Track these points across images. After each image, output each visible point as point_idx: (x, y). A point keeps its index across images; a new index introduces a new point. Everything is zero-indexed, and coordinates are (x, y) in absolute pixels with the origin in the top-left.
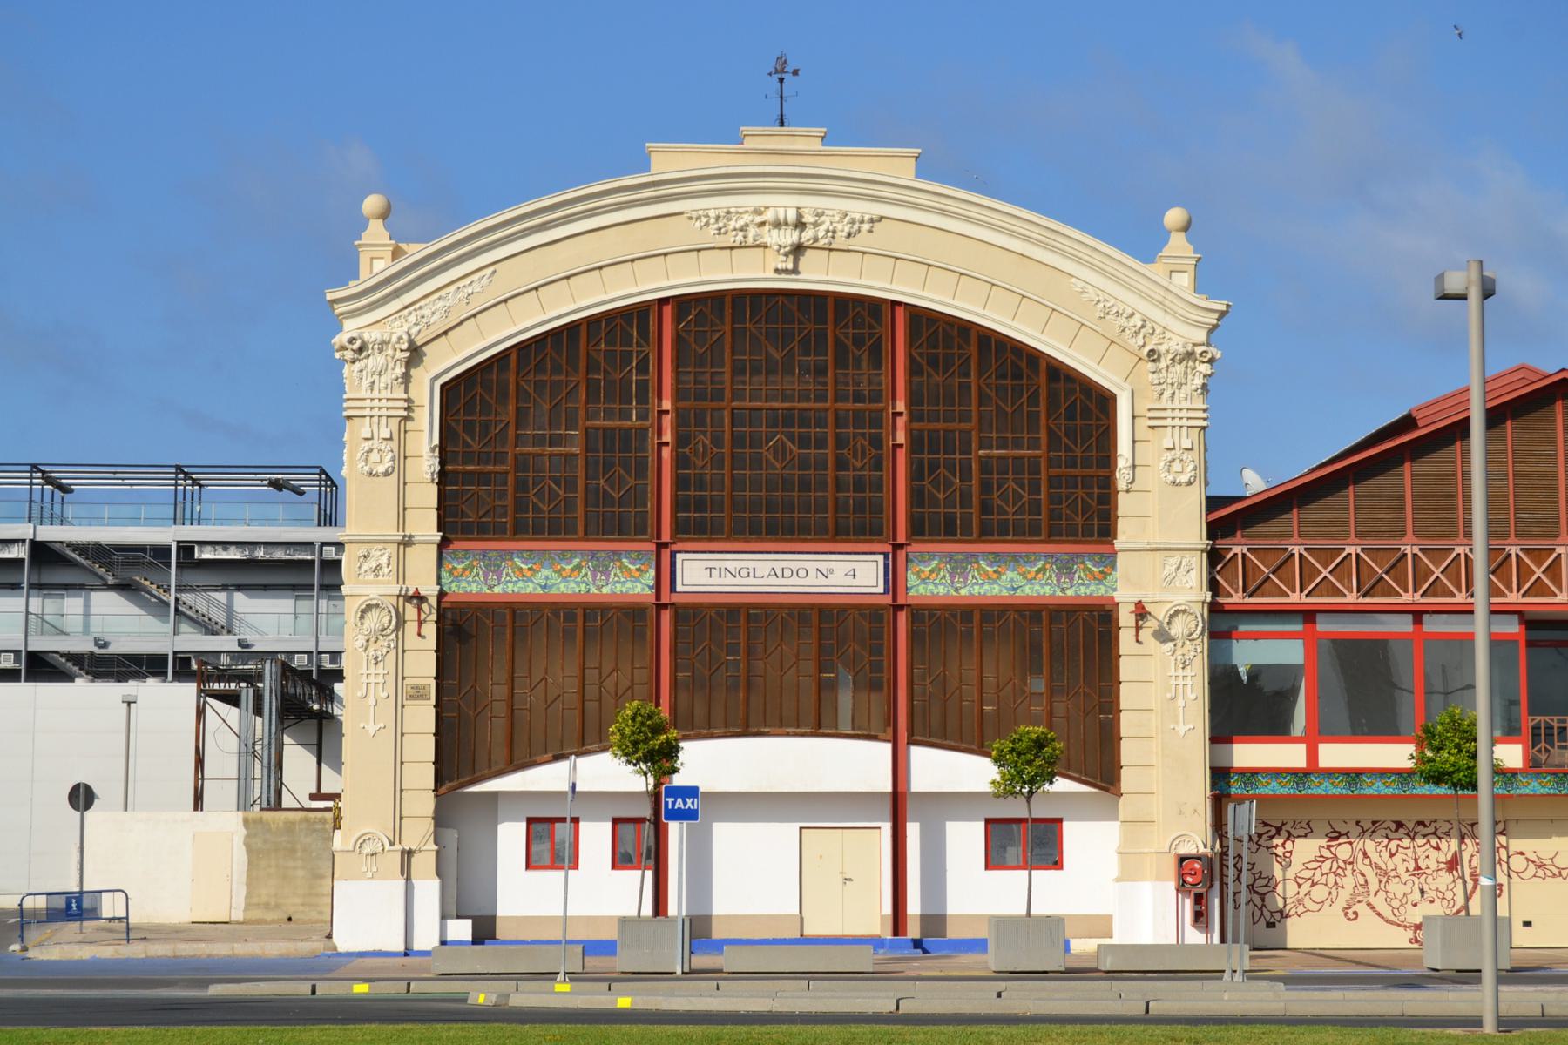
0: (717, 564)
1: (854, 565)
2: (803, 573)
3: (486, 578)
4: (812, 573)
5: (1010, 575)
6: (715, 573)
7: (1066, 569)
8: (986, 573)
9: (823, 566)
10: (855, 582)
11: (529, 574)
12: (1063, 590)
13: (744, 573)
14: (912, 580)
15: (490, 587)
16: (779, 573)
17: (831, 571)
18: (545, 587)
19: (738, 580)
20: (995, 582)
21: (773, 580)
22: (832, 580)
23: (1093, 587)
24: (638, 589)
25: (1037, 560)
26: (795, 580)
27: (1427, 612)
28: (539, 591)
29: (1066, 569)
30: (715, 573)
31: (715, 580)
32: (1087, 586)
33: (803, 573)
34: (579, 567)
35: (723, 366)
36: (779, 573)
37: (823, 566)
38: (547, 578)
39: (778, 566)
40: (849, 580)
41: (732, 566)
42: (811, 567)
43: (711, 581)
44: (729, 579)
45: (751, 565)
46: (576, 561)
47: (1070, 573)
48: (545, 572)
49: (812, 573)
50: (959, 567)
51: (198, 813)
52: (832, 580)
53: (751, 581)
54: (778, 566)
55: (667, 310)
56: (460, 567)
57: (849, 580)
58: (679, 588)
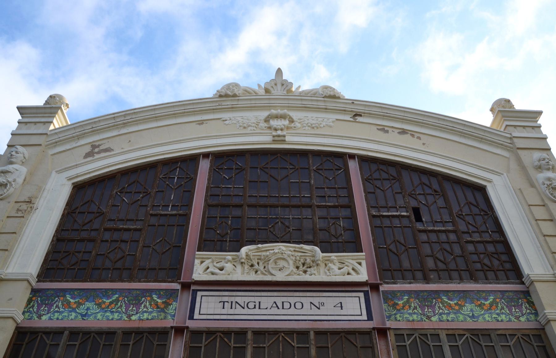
1: (341, 300)
2: (299, 305)
3: (127, 309)
4: (307, 305)
9: (316, 301)
11: (457, 308)
13: (251, 305)
16: (280, 306)
17: (323, 304)
19: (246, 311)
20: (74, 310)
21: (275, 311)
22: (323, 310)
26: (292, 311)
29: (136, 298)
32: (150, 313)
33: (299, 305)
34: (117, 300)
36: (280, 306)
37: (316, 301)
38: (88, 309)
39: (279, 301)
40: (338, 311)
42: (306, 301)
43: (224, 311)
44: (239, 310)
45: (257, 300)
46: (491, 298)
47: (138, 305)
48: (88, 304)
49: (307, 305)
50: (427, 299)
53: (257, 311)
54: (279, 301)
55: (204, 166)
56: (400, 302)
58: (196, 316)
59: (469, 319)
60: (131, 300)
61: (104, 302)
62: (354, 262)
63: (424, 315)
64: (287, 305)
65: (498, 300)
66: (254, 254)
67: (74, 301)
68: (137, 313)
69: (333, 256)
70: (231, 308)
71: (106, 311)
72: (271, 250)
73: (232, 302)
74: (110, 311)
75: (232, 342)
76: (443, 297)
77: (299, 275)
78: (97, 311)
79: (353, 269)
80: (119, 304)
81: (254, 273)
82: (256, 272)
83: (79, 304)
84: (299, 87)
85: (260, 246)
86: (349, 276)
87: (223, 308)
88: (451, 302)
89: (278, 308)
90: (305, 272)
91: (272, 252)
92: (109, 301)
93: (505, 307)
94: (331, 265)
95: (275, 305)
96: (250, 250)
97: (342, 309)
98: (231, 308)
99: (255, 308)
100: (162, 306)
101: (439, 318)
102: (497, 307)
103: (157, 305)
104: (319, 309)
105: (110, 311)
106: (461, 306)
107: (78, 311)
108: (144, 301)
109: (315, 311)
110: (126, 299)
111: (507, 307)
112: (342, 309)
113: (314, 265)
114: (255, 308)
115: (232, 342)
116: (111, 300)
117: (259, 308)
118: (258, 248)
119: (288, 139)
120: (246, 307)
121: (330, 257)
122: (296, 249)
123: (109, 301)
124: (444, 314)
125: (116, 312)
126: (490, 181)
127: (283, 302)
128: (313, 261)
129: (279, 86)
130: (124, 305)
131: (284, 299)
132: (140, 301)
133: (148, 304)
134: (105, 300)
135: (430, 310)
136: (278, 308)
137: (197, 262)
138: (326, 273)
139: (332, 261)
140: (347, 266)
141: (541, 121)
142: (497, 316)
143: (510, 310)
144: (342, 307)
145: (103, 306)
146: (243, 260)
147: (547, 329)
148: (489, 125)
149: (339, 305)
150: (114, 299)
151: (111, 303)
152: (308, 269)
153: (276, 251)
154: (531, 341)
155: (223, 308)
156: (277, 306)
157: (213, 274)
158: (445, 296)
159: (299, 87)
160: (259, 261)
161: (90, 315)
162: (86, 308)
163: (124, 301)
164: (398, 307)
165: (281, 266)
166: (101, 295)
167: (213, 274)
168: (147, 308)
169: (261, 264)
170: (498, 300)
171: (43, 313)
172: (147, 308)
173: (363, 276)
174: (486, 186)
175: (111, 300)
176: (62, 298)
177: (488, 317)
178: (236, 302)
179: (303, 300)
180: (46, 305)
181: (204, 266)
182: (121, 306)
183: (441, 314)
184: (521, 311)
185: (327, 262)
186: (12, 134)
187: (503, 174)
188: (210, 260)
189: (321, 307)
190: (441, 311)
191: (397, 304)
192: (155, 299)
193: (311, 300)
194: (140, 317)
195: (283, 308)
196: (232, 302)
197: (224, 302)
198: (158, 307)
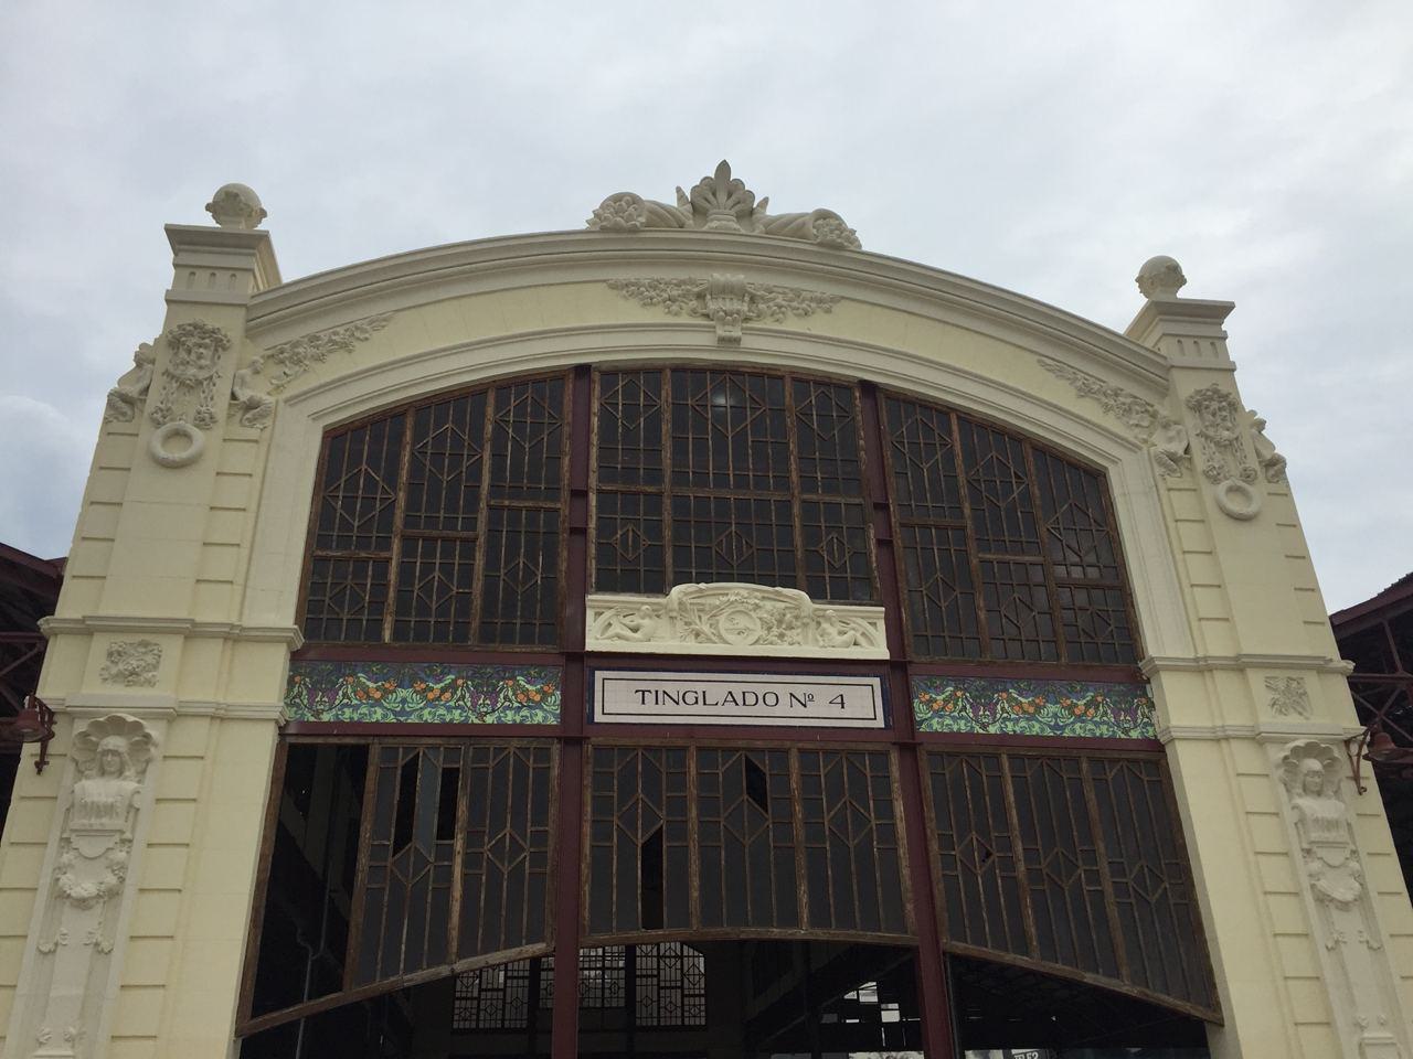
0: (653, 686)
2: (771, 700)
4: (785, 699)
5: (1052, 708)
6: (650, 698)
7: (983, 701)
8: (526, 692)
9: (799, 691)
10: (846, 713)
12: (317, 713)
13: (690, 698)
14: (921, 711)
15: (481, 716)
16: (740, 700)
18: (403, 712)
19: (683, 708)
20: (377, 703)
21: (730, 708)
22: (811, 710)
23: (1023, 723)
24: (539, 717)
25: (444, 674)
26: (760, 709)
27: (1179, 739)
28: (391, 719)
30: (650, 698)
31: (650, 707)
32: (1016, 721)
33: (771, 700)
35: (481, 869)
36: (740, 700)
37: (799, 691)
38: (404, 701)
39: (737, 690)
40: (836, 711)
41: (672, 688)
44: (669, 707)
45: (700, 687)
46: (449, 679)
48: (402, 693)
51: (38, 777)
52: (811, 710)
54: (737, 690)
56: (940, 698)
57: (836, 711)
59: (392, 717)
60: (318, 682)
61: (432, 690)
62: (864, 623)
63: (977, 722)
64: (751, 699)
65: (1100, 699)
66: (692, 601)
67: (375, 686)
68: (494, 711)
69: (831, 609)
70: (657, 703)
71: (436, 706)
72: (723, 595)
73: (657, 692)
74: (949, 715)
75: (531, 761)
76: (518, 678)
77: (771, 643)
78: (929, 715)
79: (863, 634)
80: (459, 693)
81: (693, 637)
82: (697, 635)
83: (386, 692)
84: (679, 190)
85: (703, 585)
86: (857, 648)
87: (643, 703)
88: (371, 685)
89: (737, 704)
90: (781, 636)
91: (725, 599)
92: (439, 686)
93: (968, 706)
94: (825, 625)
95: (730, 698)
96: (686, 594)
97: (843, 707)
98: (657, 703)
99: (696, 702)
100: (537, 698)
101: (338, 715)
102: (955, 705)
103: (367, 693)
104: (805, 706)
105: (949, 715)
106: (1038, 708)
107: (385, 704)
108: (503, 688)
109: (799, 710)
110: (470, 683)
111: (309, 690)
112: (843, 707)
113: (799, 624)
114: (696, 702)
115: (531, 761)
116: (442, 685)
117: (705, 704)
118: (701, 590)
119: (749, 342)
120: (681, 701)
121: (826, 610)
122: (766, 595)
123: (439, 686)
124: (1009, 720)
125: (456, 708)
126: (1115, 461)
127: (744, 693)
128: (797, 618)
129: (722, 197)
130: (467, 695)
131: (745, 687)
132: (495, 686)
133: (510, 693)
134: (431, 685)
135: (987, 713)
136: (737, 704)
137: (590, 614)
138: (817, 640)
139: (828, 619)
140: (854, 629)
141: (1229, 324)
142: (445, 712)
143: (975, 712)
144: (842, 703)
145: (935, 706)
146: (674, 614)
147: (1168, 750)
148: (1121, 330)
149: (839, 700)
150: (447, 682)
151: (443, 691)
152: (788, 633)
153: (733, 598)
154: (980, 767)
155: (643, 703)
156: (735, 701)
157: (620, 637)
158: (1014, 688)
159: (679, 190)
160: (702, 614)
161: (410, 713)
162: (399, 699)
163: (305, 684)
164: (431, 696)
165: (741, 626)
166: (423, 675)
167: (620, 637)
168: (510, 701)
169: (704, 618)
170: (959, 694)
171: (485, 710)
172: (510, 701)
173: (881, 651)
174: (1106, 468)
175: (442, 685)
176: (350, 679)
177: (938, 723)
178: (664, 692)
179: (777, 689)
180: (486, 694)
181: (611, 623)
182: (964, 708)
183: (1005, 719)
184: (994, 714)
185: (821, 620)
186: (168, 301)
187: (1140, 449)
188: (612, 612)
189: (808, 703)
190: (1005, 715)
191: (1076, 706)
192: (523, 683)
193: (791, 689)
194: (499, 718)
195: (744, 704)
196: (657, 692)
197: (643, 692)
198: (369, 697)
